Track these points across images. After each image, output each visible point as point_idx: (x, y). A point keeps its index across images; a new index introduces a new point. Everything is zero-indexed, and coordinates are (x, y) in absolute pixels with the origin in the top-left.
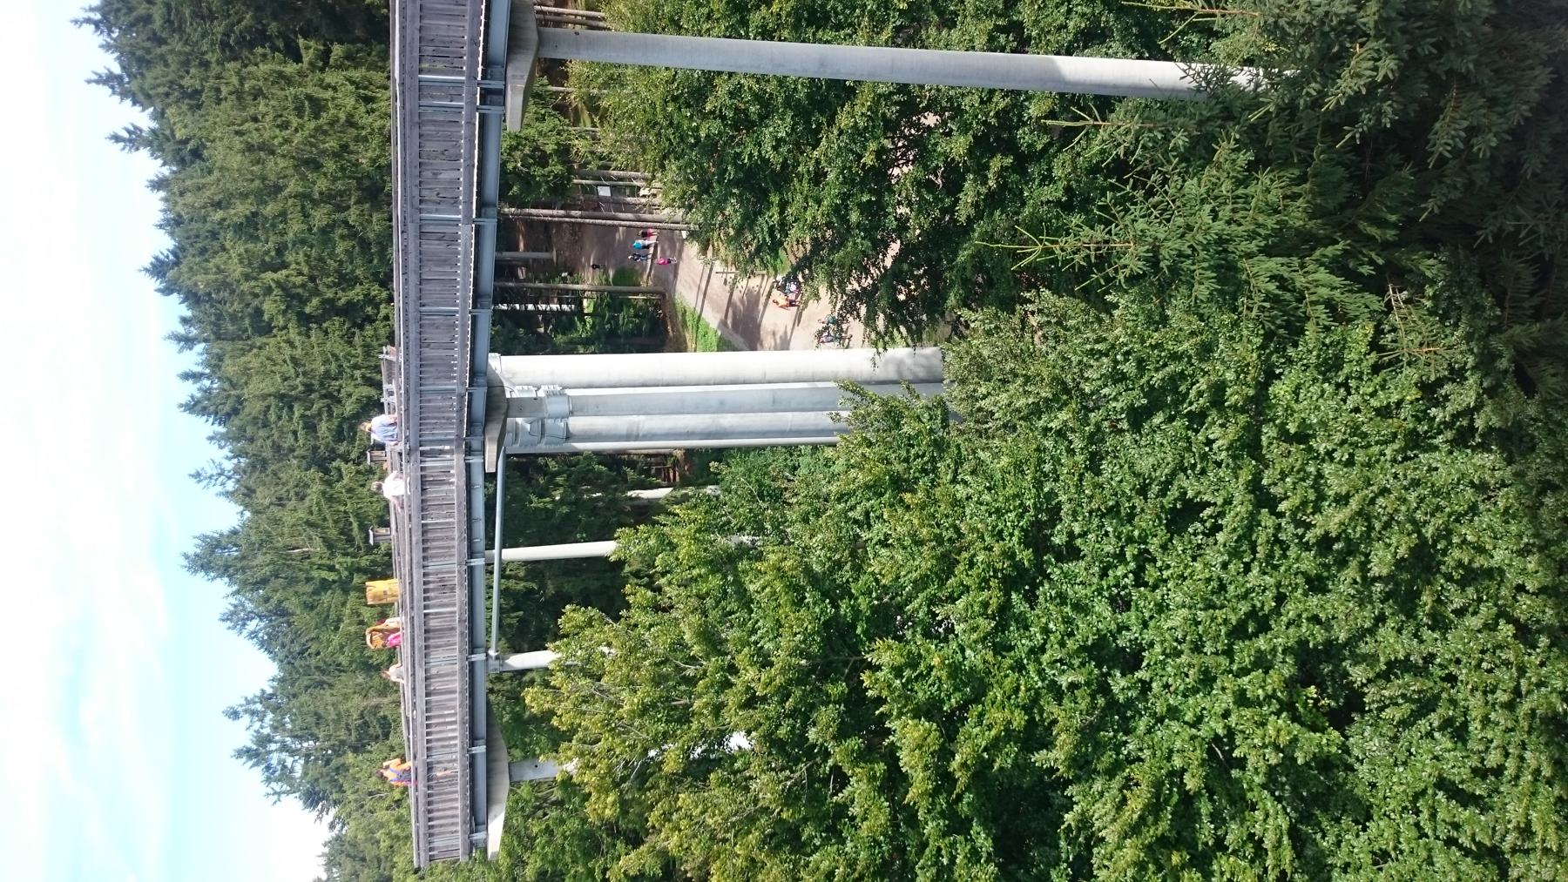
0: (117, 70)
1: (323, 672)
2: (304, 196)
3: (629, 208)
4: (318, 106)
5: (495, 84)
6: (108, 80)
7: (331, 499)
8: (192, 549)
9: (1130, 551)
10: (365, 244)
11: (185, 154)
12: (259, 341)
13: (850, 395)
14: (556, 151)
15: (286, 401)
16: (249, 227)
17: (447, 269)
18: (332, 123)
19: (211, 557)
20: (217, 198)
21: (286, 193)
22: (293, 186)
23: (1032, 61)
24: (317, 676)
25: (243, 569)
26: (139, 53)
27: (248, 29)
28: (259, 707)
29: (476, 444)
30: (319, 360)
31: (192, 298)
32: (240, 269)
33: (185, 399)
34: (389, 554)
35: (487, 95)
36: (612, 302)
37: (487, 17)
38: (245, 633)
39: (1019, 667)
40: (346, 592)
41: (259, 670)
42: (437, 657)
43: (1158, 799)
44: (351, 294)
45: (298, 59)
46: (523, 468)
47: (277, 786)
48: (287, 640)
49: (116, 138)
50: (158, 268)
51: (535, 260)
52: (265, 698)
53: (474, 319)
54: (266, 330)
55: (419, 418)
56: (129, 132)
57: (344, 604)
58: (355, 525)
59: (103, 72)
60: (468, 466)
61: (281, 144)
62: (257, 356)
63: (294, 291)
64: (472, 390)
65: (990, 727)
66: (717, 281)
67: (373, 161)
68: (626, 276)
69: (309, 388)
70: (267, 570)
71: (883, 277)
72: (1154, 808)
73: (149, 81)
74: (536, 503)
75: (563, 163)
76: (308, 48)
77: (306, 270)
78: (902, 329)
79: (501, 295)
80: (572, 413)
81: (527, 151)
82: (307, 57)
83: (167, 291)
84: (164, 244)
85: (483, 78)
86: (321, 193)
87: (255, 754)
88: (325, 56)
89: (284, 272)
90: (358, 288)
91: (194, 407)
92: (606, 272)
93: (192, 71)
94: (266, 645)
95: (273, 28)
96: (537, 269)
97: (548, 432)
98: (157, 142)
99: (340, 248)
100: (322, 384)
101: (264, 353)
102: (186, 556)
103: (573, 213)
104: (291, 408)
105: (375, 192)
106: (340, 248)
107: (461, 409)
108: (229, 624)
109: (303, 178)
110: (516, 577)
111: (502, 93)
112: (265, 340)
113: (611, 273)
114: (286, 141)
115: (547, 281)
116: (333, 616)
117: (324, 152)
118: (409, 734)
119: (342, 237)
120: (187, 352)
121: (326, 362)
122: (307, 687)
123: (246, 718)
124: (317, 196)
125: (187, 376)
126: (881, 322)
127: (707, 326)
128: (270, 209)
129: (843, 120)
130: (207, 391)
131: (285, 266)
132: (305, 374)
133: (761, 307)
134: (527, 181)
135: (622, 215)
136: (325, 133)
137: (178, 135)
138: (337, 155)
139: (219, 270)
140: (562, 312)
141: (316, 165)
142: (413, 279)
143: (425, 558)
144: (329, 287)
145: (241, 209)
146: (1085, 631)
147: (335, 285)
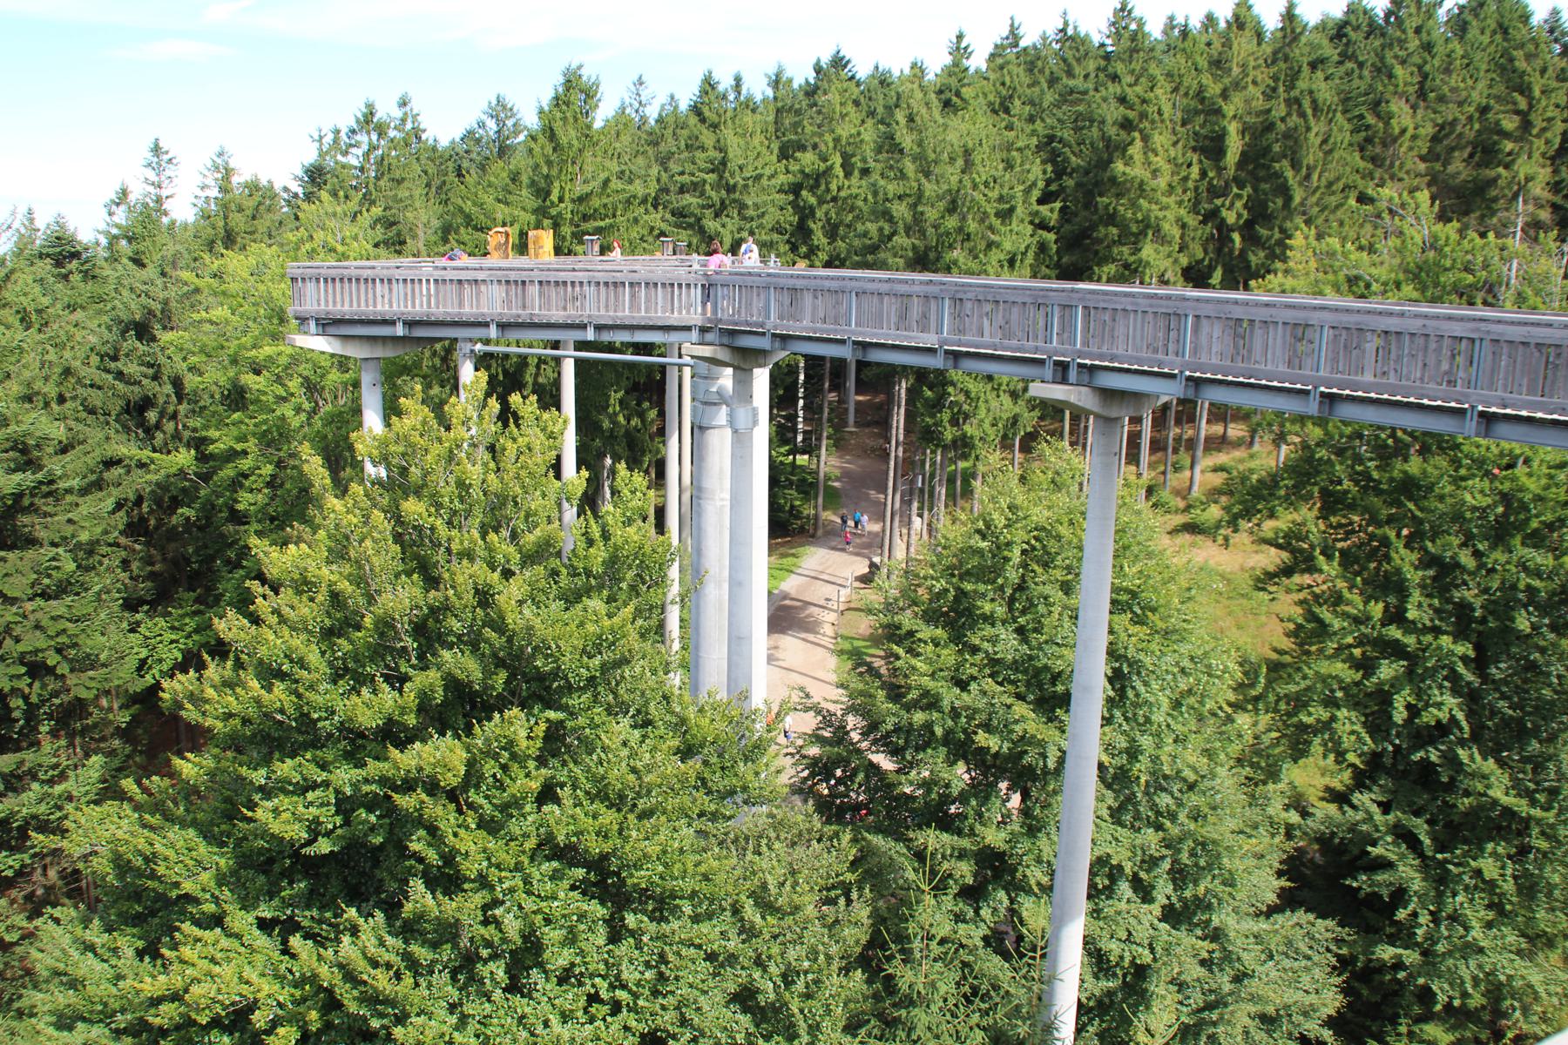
0: (1023, 44)
1: (440, 188)
2: (920, 194)
3: (907, 503)
4: (1006, 215)
5: (1073, 374)
6: (1014, 36)
7: (628, 202)
8: (586, 73)
9: (622, 995)
10: (874, 249)
11: (950, 97)
12: (775, 146)
13: (775, 709)
14: (965, 435)
15: (720, 167)
16: (889, 145)
17: (894, 319)
18: (991, 228)
19: (575, 93)
20: (918, 119)
21: (923, 180)
22: (930, 188)
23: (1082, 904)
24: (436, 182)
25: (564, 119)
26: (1040, 63)
27: (1066, 160)
28: (409, 126)
29: (709, 337)
30: (759, 200)
31: (811, 91)
32: (844, 134)
33: (716, 76)
34: (569, 253)
35: (1063, 367)
36: (807, 485)
37: (1136, 372)
38: (484, 117)
39: (518, 867)
40: (535, 211)
41: (445, 126)
42: (498, 292)
43: (381, 1003)
44: (819, 234)
45: (1040, 202)
46: (649, 386)
47: (329, 138)
48: (474, 156)
49: (960, 37)
50: (839, 62)
51: (846, 410)
52: (417, 133)
53: (843, 342)
54: (784, 154)
55: (746, 284)
56: (966, 48)
57: (523, 209)
58: (602, 224)
59: (1021, 32)
60: (688, 328)
61: (973, 181)
62: (761, 143)
63: (823, 181)
64: (768, 336)
65: (455, 835)
66: (830, 590)
67: (955, 263)
68: (833, 498)
69: (731, 189)
70: (564, 141)
71: (859, 751)
72: (374, 1000)
73: (1015, 70)
74: (615, 396)
75: (954, 442)
76: (1052, 211)
77: (843, 194)
78: (806, 773)
79: (861, 365)
80: (735, 431)
81: (966, 407)
82: (1044, 210)
83: (818, 69)
84: (862, 70)
85: (1080, 365)
86: (922, 213)
87: (368, 119)
88: (1043, 226)
89: (841, 174)
90: (825, 241)
91: (708, 85)
92: (837, 479)
93: (1028, 108)
94: (469, 135)
95: (1070, 182)
96: (839, 413)
97: (707, 408)
98: (956, 70)
99: (872, 227)
100: (735, 201)
101: (764, 150)
102: (580, 67)
103: (901, 449)
104: (712, 171)
105: (921, 261)
106: (872, 227)
107: (748, 324)
108: (494, 102)
109: (940, 198)
110: (537, 375)
111: (1064, 380)
112: (776, 151)
113: (836, 484)
114: (975, 187)
115: (829, 420)
116: (511, 198)
117: (964, 219)
118: (386, 263)
119: (881, 229)
120: (766, 81)
121: (757, 206)
122: (426, 172)
123: (398, 114)
124: (920, 209)
125: (738, 81)
126: (814, 751)
127: (783, 580)
128: (910, 167)
129: (1021, 709)
130: (724, 97)
131: (848, 175)
132: (746, 186)
133: (803, 635)
134: (937, 405)
135: (898, 497)
136: (982, 221)
137: (964, 90)
138: (960, 230)
139: (843, 116)
140: (795, 431)
141: (952, 209)
142: (884, 287)
143: (598, 284)
144: (826, 214)
145: (907, 140)
146: (552, 935)
147: (828, 220)
